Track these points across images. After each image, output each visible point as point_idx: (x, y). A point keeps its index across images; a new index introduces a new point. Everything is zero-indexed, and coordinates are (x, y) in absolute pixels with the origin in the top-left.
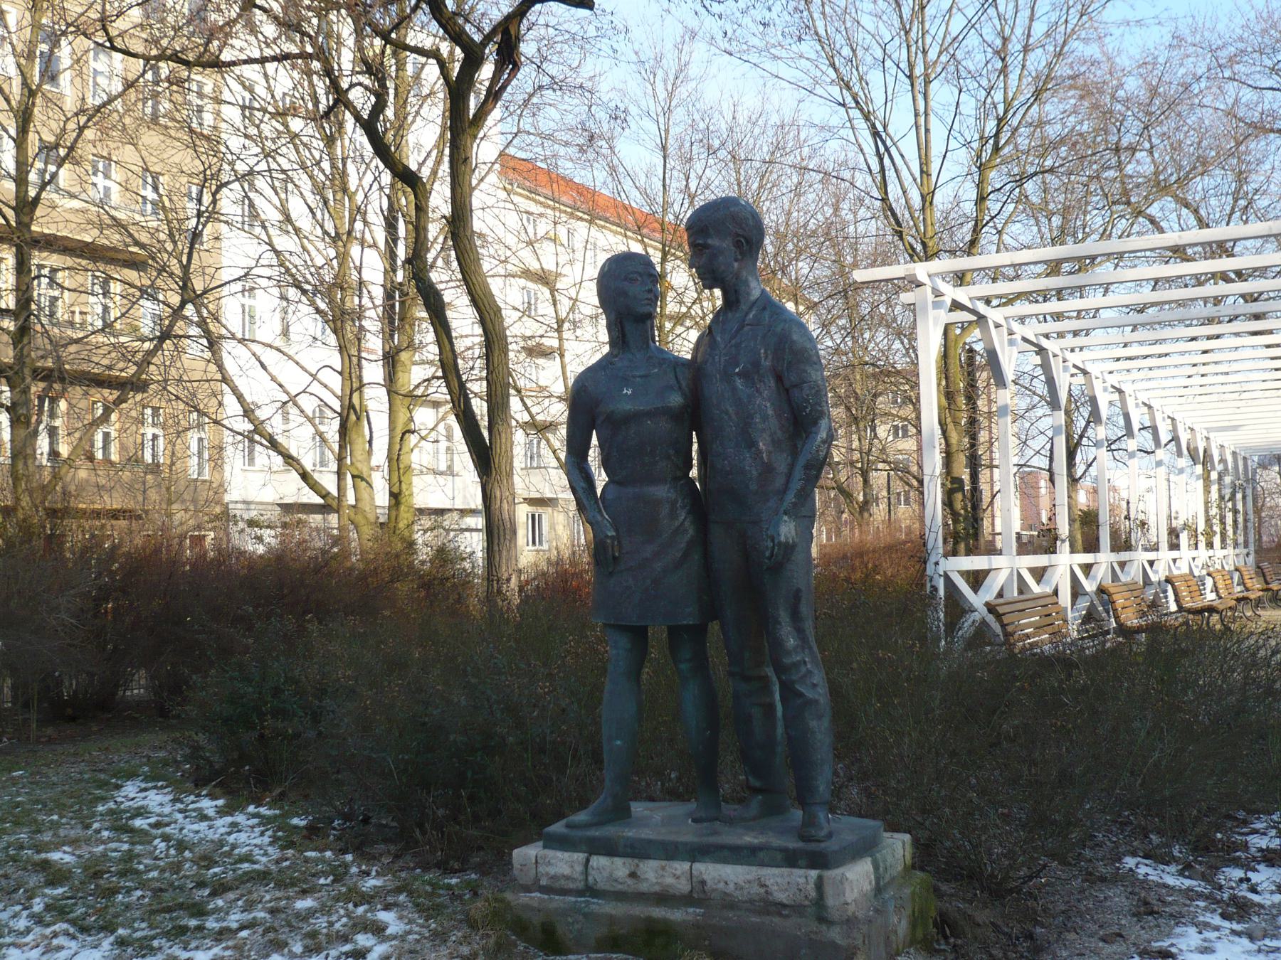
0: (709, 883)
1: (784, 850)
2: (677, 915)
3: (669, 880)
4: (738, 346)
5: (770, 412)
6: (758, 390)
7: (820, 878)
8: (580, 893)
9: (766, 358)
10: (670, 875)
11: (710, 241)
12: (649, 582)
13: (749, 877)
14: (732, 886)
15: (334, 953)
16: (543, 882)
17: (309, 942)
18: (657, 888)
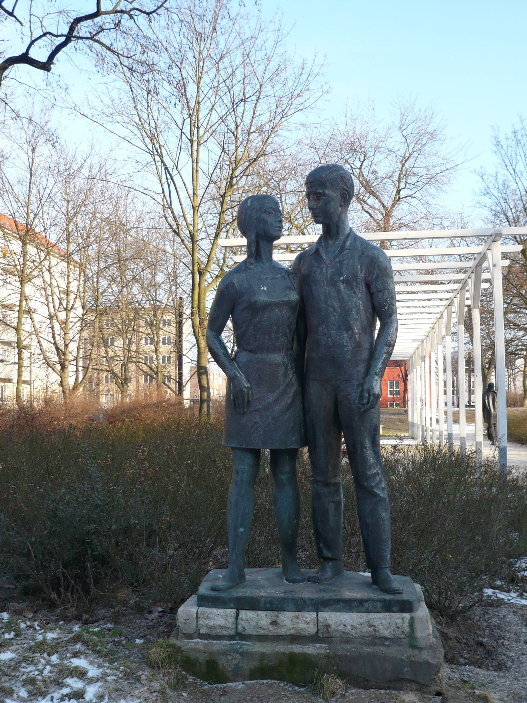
0: (333, 627)
1: (384, 601)
2: (311, 649)
3: (302, 626)
4: (340, 262)
5: (362, 308)
6: (355, 293)
7: (412, 619)
8: (231, 638)
9: (361, 271)
10: (305, 621)
11: (327, 192)
12: (270, 419)
13: (361, 621)
14: (349, 627)
15: (57, 695)
16: (203, 631)
17: (30, 687)
18: (292, 632)
